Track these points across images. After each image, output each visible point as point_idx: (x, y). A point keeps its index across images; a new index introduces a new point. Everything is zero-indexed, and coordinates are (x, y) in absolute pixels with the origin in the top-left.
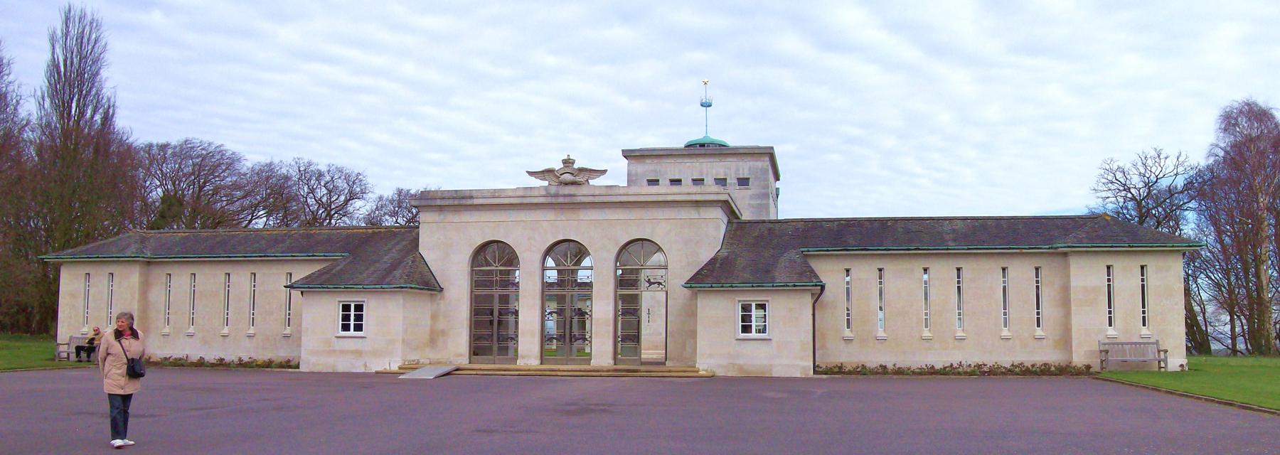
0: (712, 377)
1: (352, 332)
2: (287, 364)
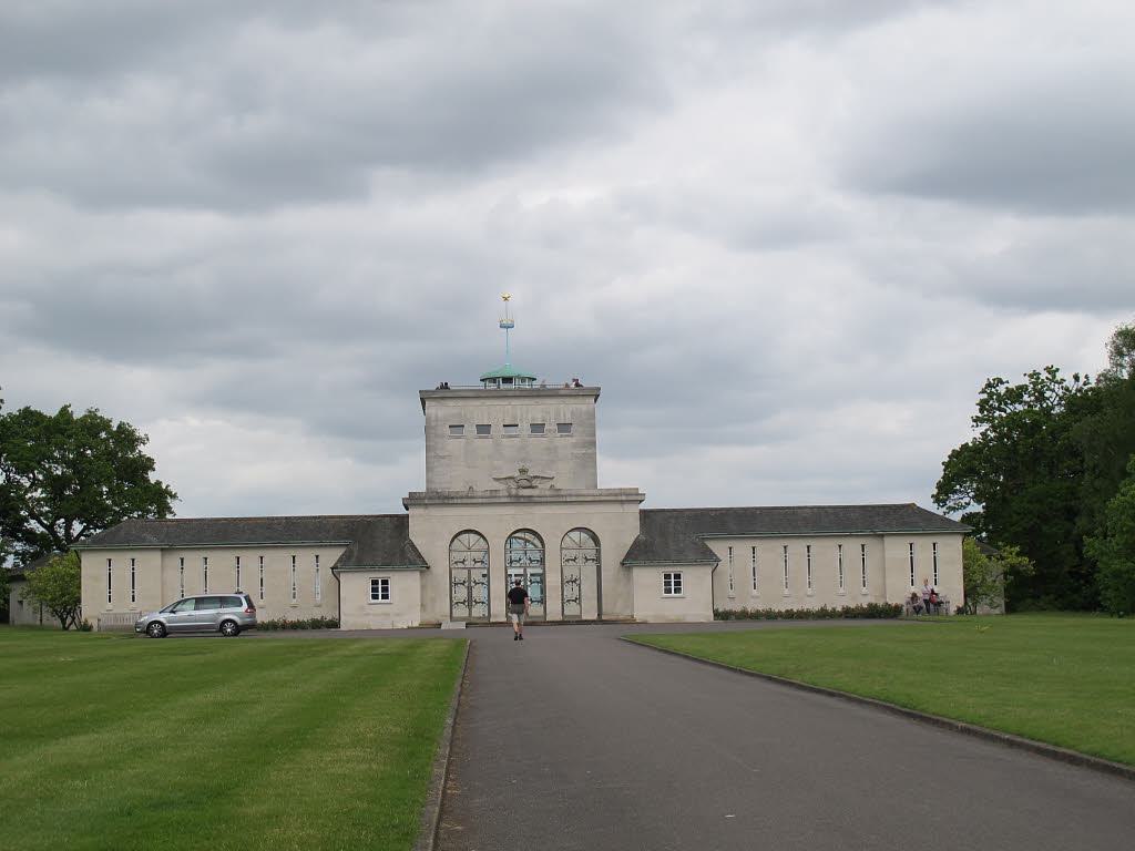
0: (645, 623)
2: (335, 624)
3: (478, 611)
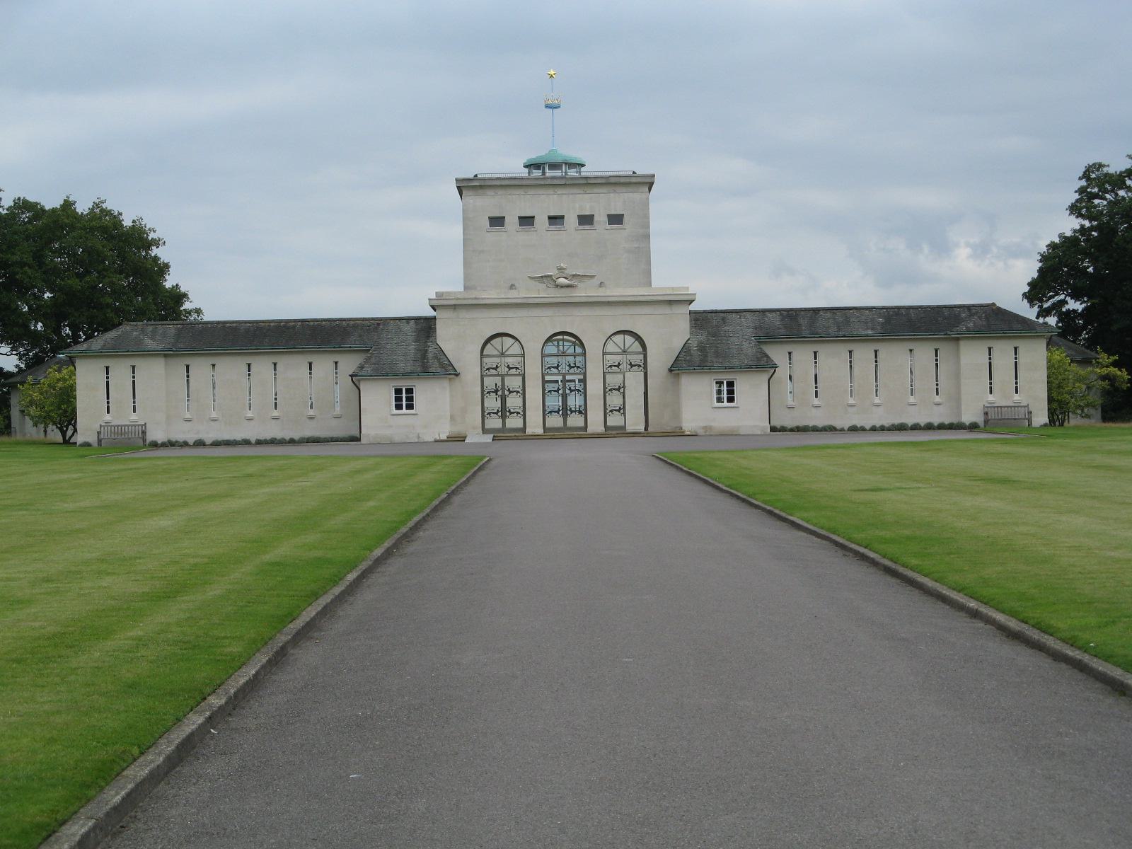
1: (404, 411)
3: (514, 422)
